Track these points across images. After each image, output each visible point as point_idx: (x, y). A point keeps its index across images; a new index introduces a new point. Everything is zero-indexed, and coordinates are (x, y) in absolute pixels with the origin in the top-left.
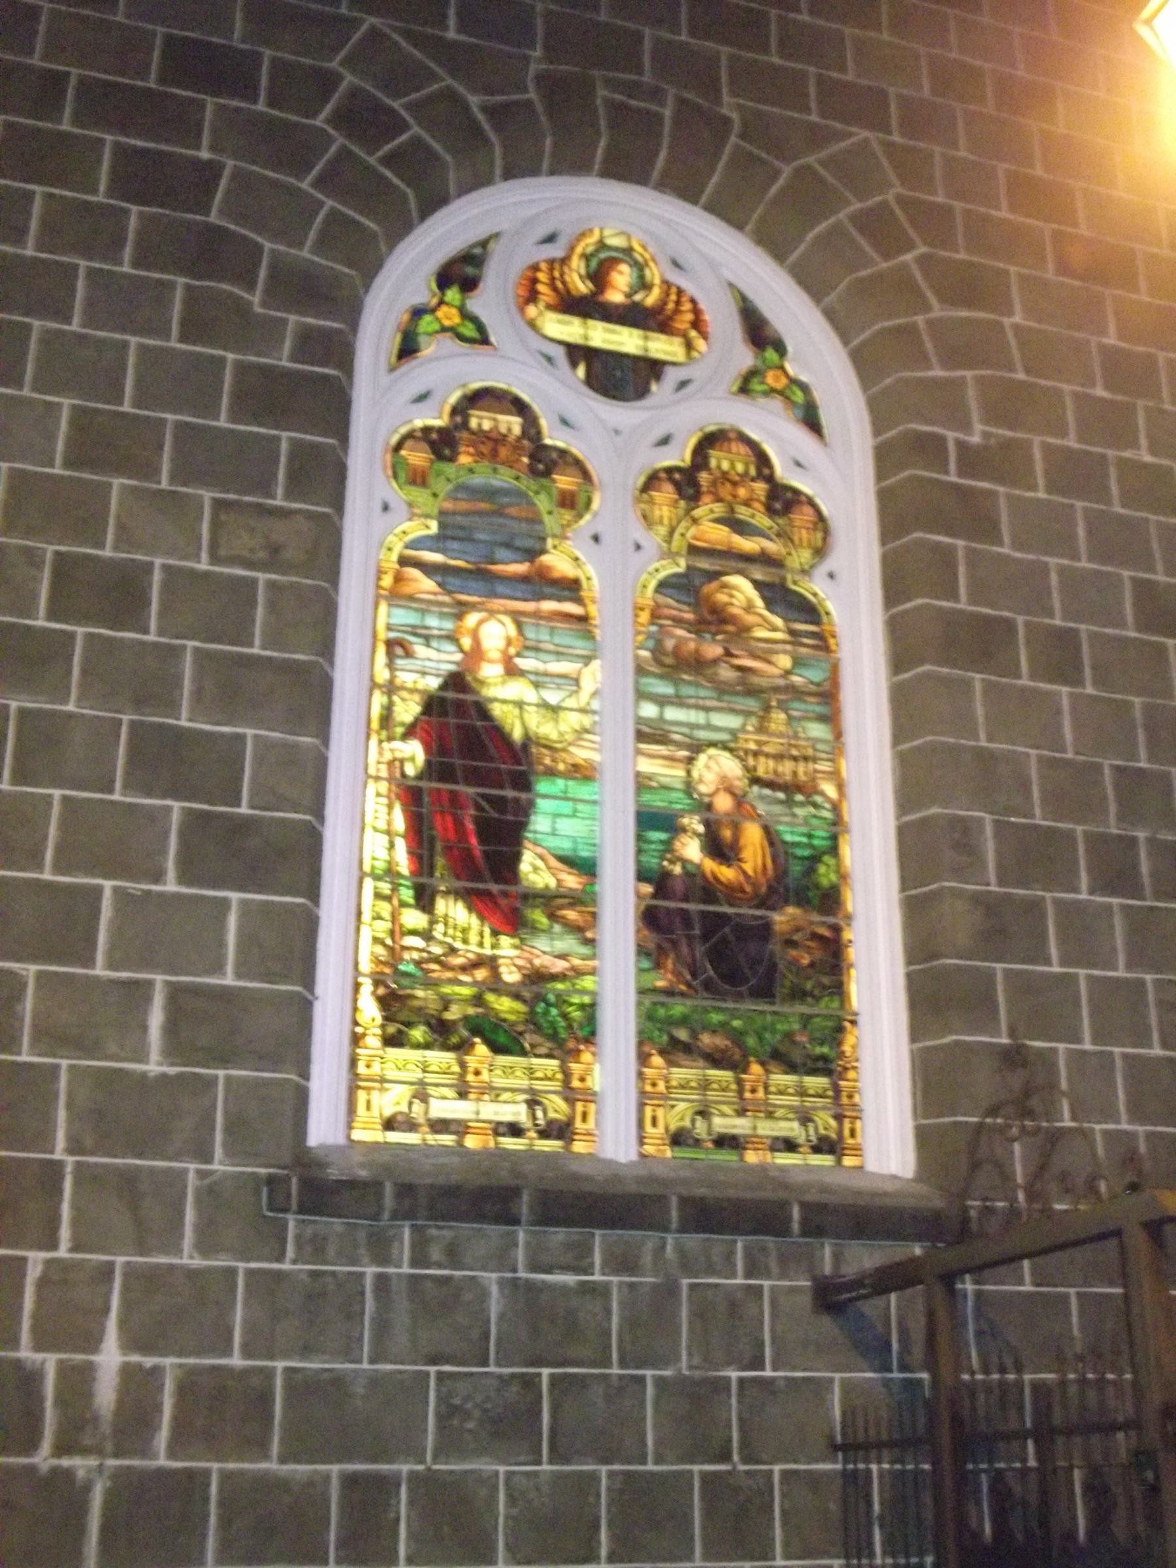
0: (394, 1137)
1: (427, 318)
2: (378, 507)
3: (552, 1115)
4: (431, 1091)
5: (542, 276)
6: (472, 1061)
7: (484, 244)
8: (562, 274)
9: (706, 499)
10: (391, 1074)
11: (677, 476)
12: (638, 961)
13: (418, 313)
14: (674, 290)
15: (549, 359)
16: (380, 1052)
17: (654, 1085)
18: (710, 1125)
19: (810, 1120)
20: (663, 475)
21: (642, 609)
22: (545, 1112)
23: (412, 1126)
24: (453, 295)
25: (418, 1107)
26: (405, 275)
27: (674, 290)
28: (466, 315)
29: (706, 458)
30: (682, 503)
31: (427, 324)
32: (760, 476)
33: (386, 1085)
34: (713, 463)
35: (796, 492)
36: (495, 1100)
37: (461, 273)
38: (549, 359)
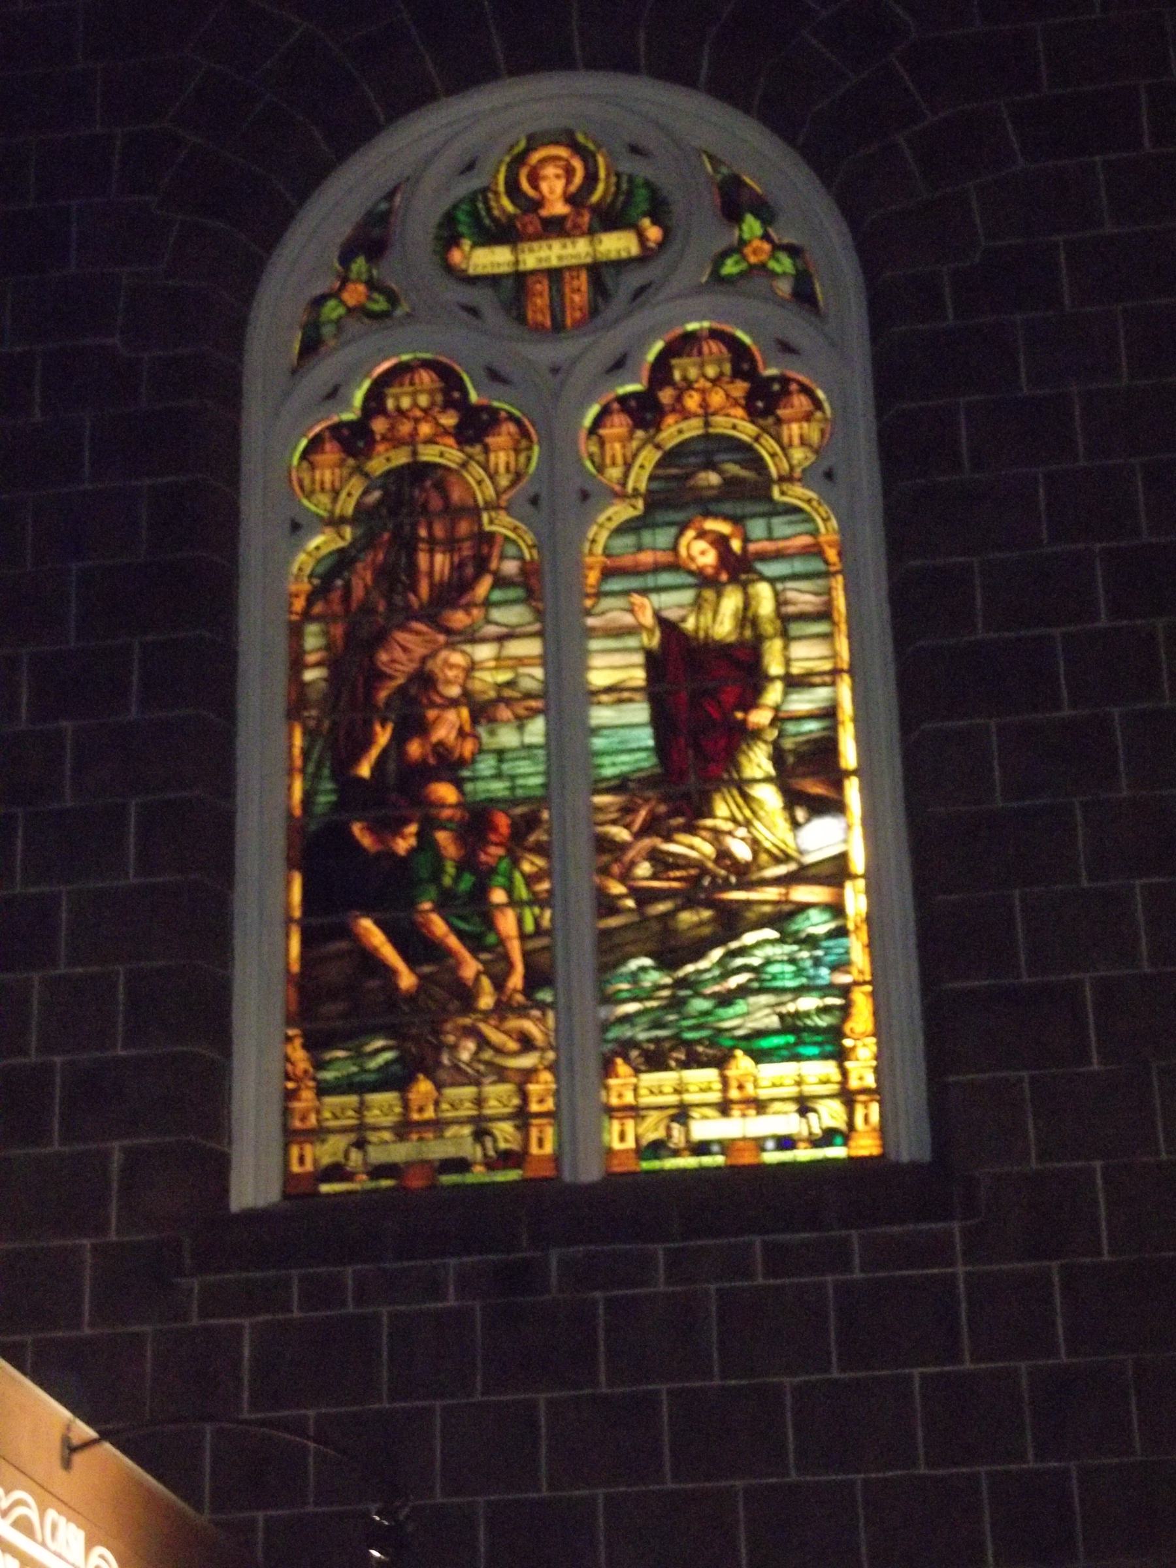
0: (502, 1177)
1: (332, 303)
2: (544, 503)
3: (503, 1145)
4: (373, 1137)
5: (462, 217)
6: (732, 1072)
7: (390, 196)
8: (616, 194)
9: (381, 448)
10: (646, 1100)
11: (776, 387)
12: (552, 966)
13: (319, 302)
14: (625, 179)
15: (473, 311)
16: (634, 1080)
17: (620, 1096)
18: (687, 1133)
19: (489, 1133)
20: (616, 406)
21: (297, 596)
22: (495, 1140)
23: (348, 1177)
24: (359, 265)
25: (355, 1156)
26: (304, 258)
27: (625, 179)
28: (372, 285)
29: (669, 369)
30: (351, 462)
31: (332, 310)
32: (737, 374)
33: (643, 1113)
34: (390, 404)
35: (496, 411)
36: (440, 1136)
37: (371, 240)
38: (473, 311)
